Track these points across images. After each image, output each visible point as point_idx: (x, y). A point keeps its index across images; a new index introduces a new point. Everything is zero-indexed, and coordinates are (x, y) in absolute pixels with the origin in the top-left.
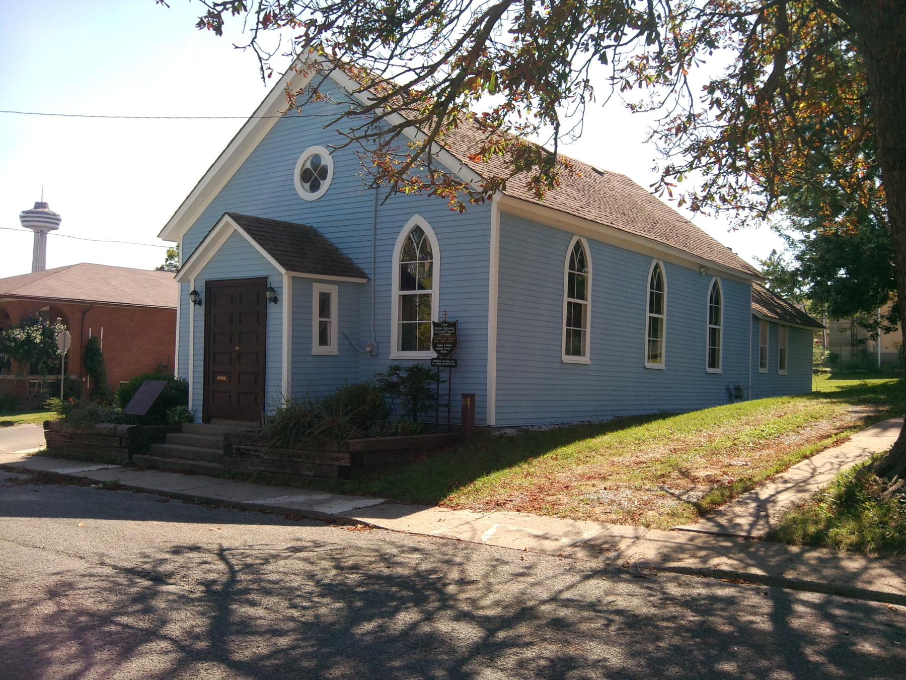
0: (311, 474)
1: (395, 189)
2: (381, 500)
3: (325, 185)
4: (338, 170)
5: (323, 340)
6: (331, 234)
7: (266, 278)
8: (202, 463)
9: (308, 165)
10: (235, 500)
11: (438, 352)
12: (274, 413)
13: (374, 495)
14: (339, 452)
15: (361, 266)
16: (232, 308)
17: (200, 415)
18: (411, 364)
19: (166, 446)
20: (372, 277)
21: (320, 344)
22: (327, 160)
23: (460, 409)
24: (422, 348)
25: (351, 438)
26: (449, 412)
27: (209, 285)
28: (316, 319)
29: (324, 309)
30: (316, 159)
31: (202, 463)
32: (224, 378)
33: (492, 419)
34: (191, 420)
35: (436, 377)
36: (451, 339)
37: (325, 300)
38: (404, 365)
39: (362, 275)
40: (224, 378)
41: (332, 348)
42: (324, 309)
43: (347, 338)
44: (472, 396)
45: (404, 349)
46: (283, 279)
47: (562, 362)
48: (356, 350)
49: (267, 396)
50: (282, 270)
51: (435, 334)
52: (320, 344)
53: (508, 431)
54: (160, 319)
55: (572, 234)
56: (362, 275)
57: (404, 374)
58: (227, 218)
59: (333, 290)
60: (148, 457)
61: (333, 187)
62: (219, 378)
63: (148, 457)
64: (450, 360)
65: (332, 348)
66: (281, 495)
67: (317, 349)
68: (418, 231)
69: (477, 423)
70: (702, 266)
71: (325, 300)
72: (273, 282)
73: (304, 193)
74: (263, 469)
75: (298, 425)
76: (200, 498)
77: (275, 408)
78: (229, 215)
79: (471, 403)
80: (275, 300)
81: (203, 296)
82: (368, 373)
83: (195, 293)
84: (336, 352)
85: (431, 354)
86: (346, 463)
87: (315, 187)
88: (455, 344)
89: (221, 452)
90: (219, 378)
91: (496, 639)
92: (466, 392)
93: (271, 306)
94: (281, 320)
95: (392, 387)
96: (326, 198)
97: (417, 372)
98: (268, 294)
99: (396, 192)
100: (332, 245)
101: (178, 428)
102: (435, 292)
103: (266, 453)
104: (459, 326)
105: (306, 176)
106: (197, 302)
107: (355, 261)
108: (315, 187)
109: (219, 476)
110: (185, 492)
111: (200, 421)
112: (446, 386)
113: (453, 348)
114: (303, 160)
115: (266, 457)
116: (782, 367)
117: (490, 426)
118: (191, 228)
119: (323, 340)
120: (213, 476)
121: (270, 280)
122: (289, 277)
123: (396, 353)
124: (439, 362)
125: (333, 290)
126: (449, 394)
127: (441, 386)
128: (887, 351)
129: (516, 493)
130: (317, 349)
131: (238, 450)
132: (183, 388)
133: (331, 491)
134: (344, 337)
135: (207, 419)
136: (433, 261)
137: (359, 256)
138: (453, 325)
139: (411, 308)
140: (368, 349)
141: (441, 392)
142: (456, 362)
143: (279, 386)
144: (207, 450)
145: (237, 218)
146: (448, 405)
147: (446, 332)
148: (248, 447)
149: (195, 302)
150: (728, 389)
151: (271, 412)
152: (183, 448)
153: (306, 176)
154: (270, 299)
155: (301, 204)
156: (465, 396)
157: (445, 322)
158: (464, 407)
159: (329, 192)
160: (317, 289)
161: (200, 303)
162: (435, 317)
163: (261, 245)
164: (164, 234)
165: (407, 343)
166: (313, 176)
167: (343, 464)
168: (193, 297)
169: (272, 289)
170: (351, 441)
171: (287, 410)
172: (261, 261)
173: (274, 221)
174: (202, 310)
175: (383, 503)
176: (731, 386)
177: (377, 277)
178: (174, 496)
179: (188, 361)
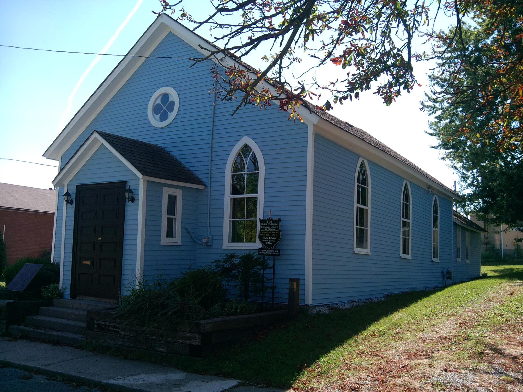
0: (164, 350)
1: (245, 101)
2: (233, 382)
3: (172, 116)
4: (181, 104)
5: (170, 234)
6: (176, 152)
7: (125, 183)
8: (68, 335)
9: (159, 101)
10: (96, 378)
11: (264, 243)
12: (128, 294)
13: (228, 376)
14: (190, 332)
15: (200, 176)
16: (96, 206)
17: (68, 291)
18: (244, 253)
19: (39, 318)
20: (208, 185)
21: (167, 237)
22: (174, 96)
23: (287, 291)
24: (252, 240)
25: (201, 319)
26: (273, 293)
27: (80, 188)
28: (165, 216)
29: (172, 210)
30: (165, 97)
31: (68, 335)
32: (88, 263)
33: (309, 300)
34: (61, 295)
35: (264, 265)
36: (275, 233)
37: (172, 200)
38: (238, 253)
39: (199, 182)
40: (88, 263)
41: (177, 240)
42: (172, 210)
43: (189, 232)
44: (297, 280)
45: (233, 241)
46: (139, 182)
47: (354, 253)
48: (195, 242)
49: (123, 277)
50: (139, 175)
51: (261, 229)
52: (167, 237)
53: (320, 308)
54: (45, 219)
55: (359, 156)
56: (199, 182)
57: (237, 261)
58: (96, 135)
59: (179, 194)
60: (22, 327)
61: (180, 112)
62: (84, 262)
63: (22, 327)
64: (274, 250)
65: (177, 240)
66: (139, 374)
67: (164, 240)
68: (246, 149)
69: (301, 302)
70: (429, 187)
71: (172, 200)
72: (131, 185)
73: (155, 122)
74: (120, 343)
75: (151, 303)
76: (62, 375)
77: (131, 289)
78: (97, 132)
79: (296, 284)
80: (133, 200)
81: (74, 197)
82: (206, 260)
83: (67, 194)
84: (179, 243)
85: (257, 245)
86: (197, 342)
87: (164, 117)
88: (278, 237)
89: (84, 325)
90: (84, 262)
91: (126, 292)
92: (293, 277)
93: (129, 205)
94: (137, 216)
95: (226, 272)
96: (172, 125)
97: (248, 259)
98: (127, 195)
99: (246, 103)
100: (177, 160)
101: (50, 303)
102: (260, 196)
103: (124, 330)
104: (282, 223)
105: (156, 109)
106: (69, 202)
107: (195, 173)
108: (164, 117)
109: (81, 348)
110: (50, 368)
111: (67, 297)
112: (271, 271)
113: (276, 240)
114: (155, 98)
115: (123, 333)
116: (467, 259)
117: (308, 305)
118: (66, 149)
119: (170, 234)
120: (76, 348)
121: (128, 184)
122: (144, 181)
123: (227, 244)
124: (264, 252)
125: (179, 194)
126: (274, 278)
127: (266, 271)
128: (507, 248)
129: (363, 375)
130: (164, 240)
131: (99, 325)
132: (56, 268)
133: (184, 368)
134: (185, 230)
135: (73, 296)
136: (259, 171)
137: (199, 169)
138: (277, 221)
139: (243, 208)
140: (204, 241)
141: (266, 276)
142: (279, 251)
143: (134, 270)
144: (73, 323)
145: (104, 135)
146: (273, 288)
147: (271, 228)
148: (107, 324)
149: (67, 201)
150: (443, 273)
151: (126, 292)
152: (54, 320)
153: (156, 109)
154: (129, 198)
155: (153, 128)
156: (291, 280)
157: (270, 219)
158: (291, 290)
159: (174, 122)
160: (166, 192)
161: (71, 203)
162: (260, 214)
163: (123, 155)
164: (48, 154)
165: (236, 237)
166: (163, 108)
167: (193, 343)
168: (66, 198)
169: (130, 191)
170: (202, 322)
171: (141, 291)
172: (123, 169)
173: (133, 140)
174: (72, 208)
175: (236, 386)
176: (444, 271)
177: (213, 184)
178: (39, 371)
179: (61, 249)
